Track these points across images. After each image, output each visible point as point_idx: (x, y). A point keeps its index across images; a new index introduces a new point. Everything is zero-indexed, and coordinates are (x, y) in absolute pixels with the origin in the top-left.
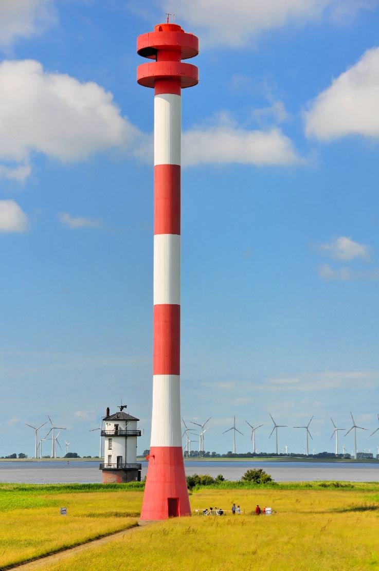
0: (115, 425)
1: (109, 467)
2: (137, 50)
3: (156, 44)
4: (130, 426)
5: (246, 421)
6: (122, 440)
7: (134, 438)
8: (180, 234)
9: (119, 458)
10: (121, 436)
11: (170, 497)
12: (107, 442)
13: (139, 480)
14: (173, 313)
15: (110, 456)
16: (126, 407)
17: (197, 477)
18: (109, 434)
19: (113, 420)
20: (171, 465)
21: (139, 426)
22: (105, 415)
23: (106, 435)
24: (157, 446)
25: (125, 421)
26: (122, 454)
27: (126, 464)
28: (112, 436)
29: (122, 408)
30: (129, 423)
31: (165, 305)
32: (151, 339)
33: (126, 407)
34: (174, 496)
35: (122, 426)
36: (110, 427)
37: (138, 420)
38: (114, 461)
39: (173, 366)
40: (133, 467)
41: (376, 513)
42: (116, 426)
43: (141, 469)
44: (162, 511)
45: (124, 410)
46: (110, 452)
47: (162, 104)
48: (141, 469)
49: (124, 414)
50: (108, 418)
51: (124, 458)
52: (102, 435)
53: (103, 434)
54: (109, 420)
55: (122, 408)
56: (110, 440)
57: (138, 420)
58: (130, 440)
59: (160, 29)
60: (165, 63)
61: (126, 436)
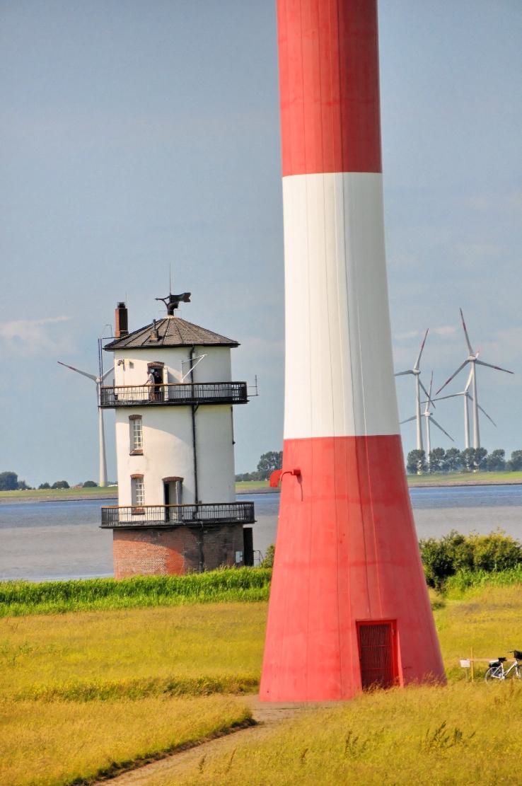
6: (181, 416)
9: (170, 485)
10: (175, 403)
11: (363, 616)
12: (122, 429)
15: (137, 480)
16: (186, 297)
20: (363, 501)
21: (239, 367)
22: (112, 332)
23: (118, 406)
26: (181, 469)
28: (143, 405)
29: (174, 302)
30: (202, 356)
33: (186, 297)
34: (379, 614)
35: (175, 369)
36: (132, 375)
38: (153, 495)
39: (353, 140)
40: (212, 516)
42: (156, 372)
43: (253, 521)
44: (339, 669)
45: (182, 310)
48: (253, 521)
50: (122, 342)
51: (188, 484)
52: (105, 406)
53: (109, 400)
54: (125, 349)
55: (174, 302)
57: (235, 345)
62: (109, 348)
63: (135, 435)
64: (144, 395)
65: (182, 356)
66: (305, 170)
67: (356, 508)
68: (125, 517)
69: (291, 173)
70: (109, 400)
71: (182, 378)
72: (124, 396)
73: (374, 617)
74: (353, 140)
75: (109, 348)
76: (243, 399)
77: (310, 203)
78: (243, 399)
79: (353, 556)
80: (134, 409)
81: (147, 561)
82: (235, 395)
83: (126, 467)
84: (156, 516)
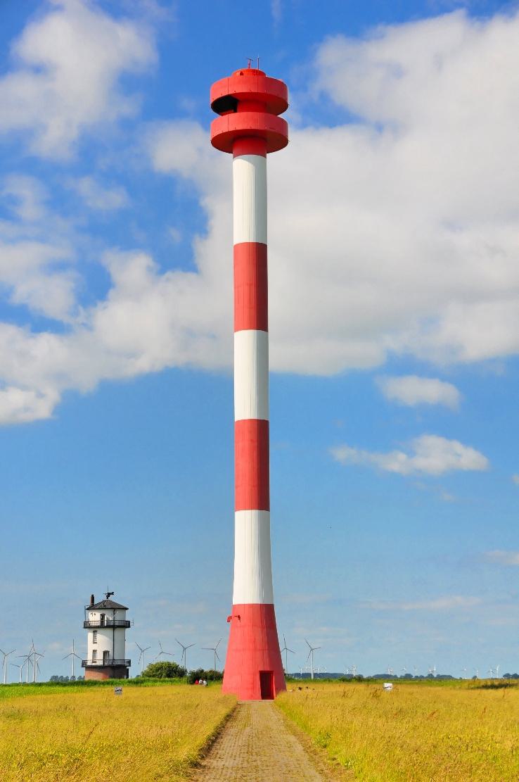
0: (101, 615)
1: (94, 664)
2: (211, 102)
3: (237, 92)
4: (119, 616)
5: (176, 639)
6: (110, 631)
7: (121, 630)
8: (267, 331)
9: (105, 653)
10: (108, 627)
11: (262, 669)
12: (90, 635)
13: (128, 677)
14: (261, 429)
15: (95, 651)
16: (113, 593)
17: (202, 671)
18: (93, 625)
19: (99, 609)
20: (263, 628)
21: (128, 616)
22: (89, 603)
23: (90, 627)
24: (247, 602)
25: (113, 610)
26: (109, 648)
27: (114, 660)
28: (98, 627)
29: (109, 595)
30: (118, 612)
31: (251, 420)
32: (240, 464)
33: (113, 593)
34: (267, 669)
35: (109, 616)
36: (95, 618)
37: (127, 609)
38: (100, 656)
39: (262, 501)
40: (119, 663)
41: (514, 693)
42: (103, 616)
43: (130, 666)
44: (253, 688)
45: (111, 598)
46: (95, 647)
47: (241, 167)
48: (130, 666)
49: (111, 602)
50: (93, 607)
51: (111, 653)
52: (85, 627)
53: (87, 626)
54: (94, 609)
55: (109, 595)
56: (95, 632)
57: (127, 609)
58: (118, 632)
59: (242, 74)
60: (250, 114)
61: (113, 627)
62: (88, 609)
63: (95, 637)
64: (99, 624)
65: (111, 612)
66: (245, 509)
67: (260, 630)
68: (89, 663)
69: (239, 510)
70: (87, 626)
71: (111, 619)
72: (93, 624)
73: (266, 670)
74: (262, 501)
75: (88, 609)
76: (129, 627)
77: (245, 522)
78: (129, 627)
79: (258, 647)
80: (95, 629)
81: (96, 676)
82: (126, 625)
83: (91, 647)
84: (100, 663)
